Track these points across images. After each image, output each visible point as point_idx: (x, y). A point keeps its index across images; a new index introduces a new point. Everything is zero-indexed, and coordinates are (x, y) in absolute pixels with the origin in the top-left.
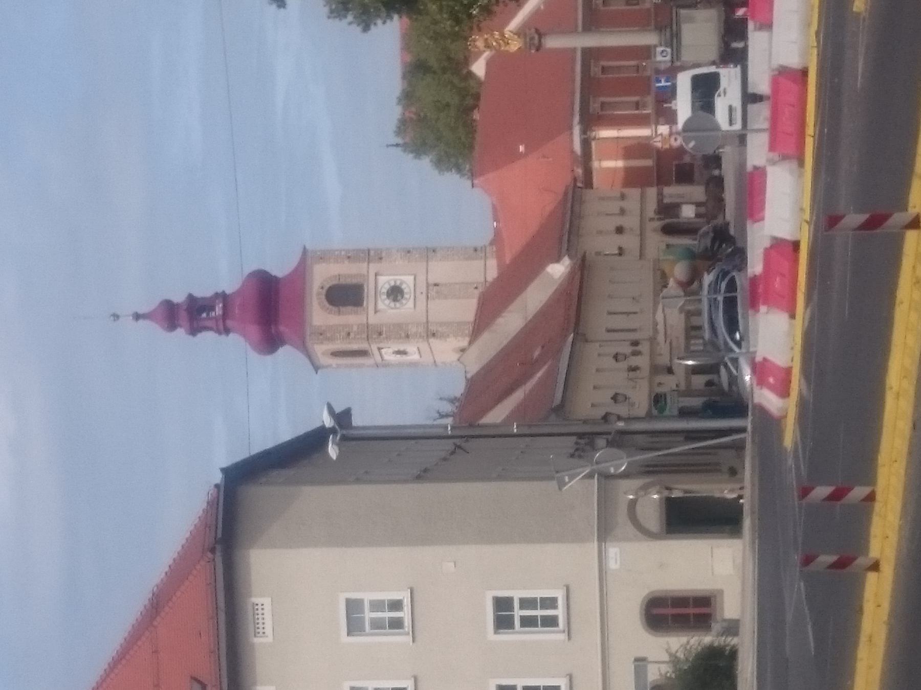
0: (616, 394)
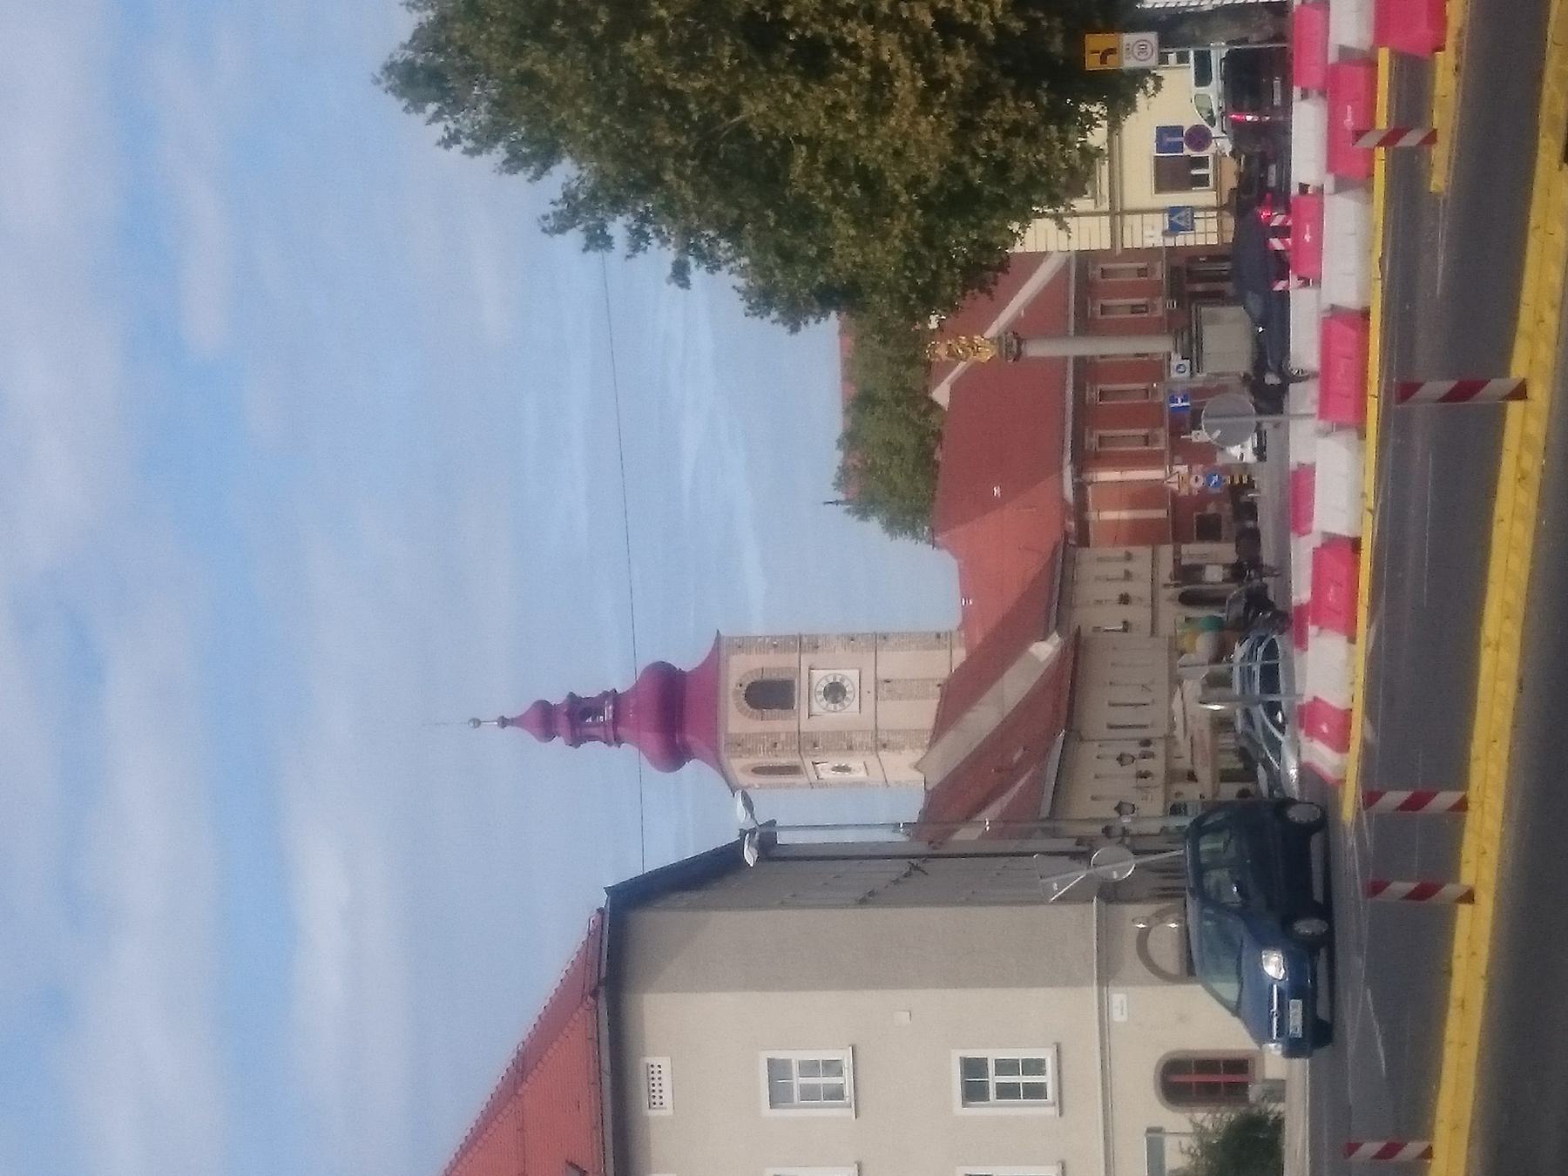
0: (1121, 804)
